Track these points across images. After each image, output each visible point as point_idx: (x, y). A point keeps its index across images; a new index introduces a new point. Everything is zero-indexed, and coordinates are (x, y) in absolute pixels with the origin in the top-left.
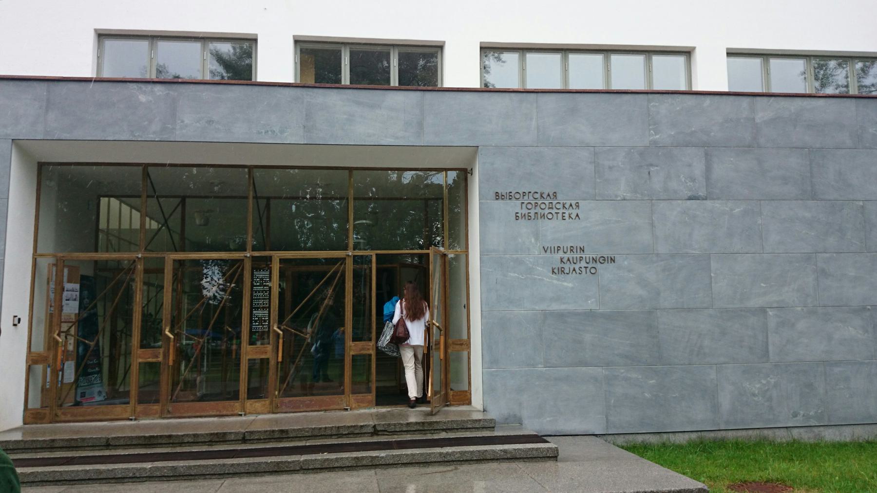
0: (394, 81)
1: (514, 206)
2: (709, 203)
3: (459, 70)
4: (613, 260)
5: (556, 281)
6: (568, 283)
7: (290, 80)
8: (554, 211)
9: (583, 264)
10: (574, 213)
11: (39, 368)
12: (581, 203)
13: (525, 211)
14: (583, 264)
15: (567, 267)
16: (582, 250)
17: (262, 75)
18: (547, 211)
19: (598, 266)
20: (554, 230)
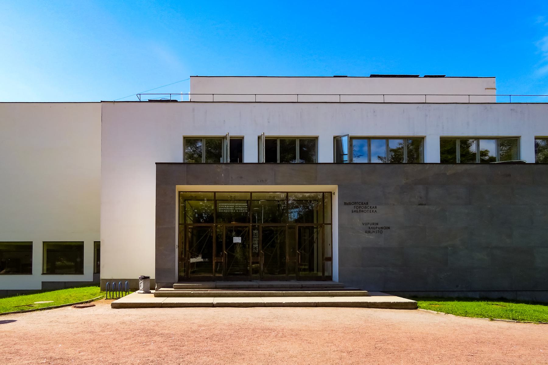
0: (458, 161)
1: (352, 207)
2: (426, 207)
3: (325, 154)
4: (389, 228)
5: (367, 235)
6: (371, 237)
7: (182, 161)
8: (367, 209)
9: (377, 229)
10: (374, 210)
11: (329, 222)
12: (377, 206)
13: (356, 209)
14: (377, 229)
15: (371, 230)
16: (377, 224)
17: (321, 160)
18: (364, 209)
19: (383, 230)
20: (367, 217)
